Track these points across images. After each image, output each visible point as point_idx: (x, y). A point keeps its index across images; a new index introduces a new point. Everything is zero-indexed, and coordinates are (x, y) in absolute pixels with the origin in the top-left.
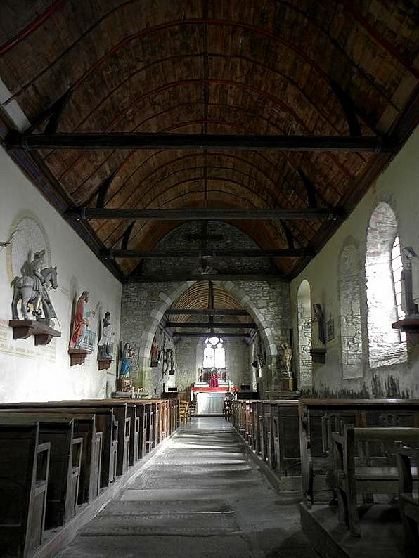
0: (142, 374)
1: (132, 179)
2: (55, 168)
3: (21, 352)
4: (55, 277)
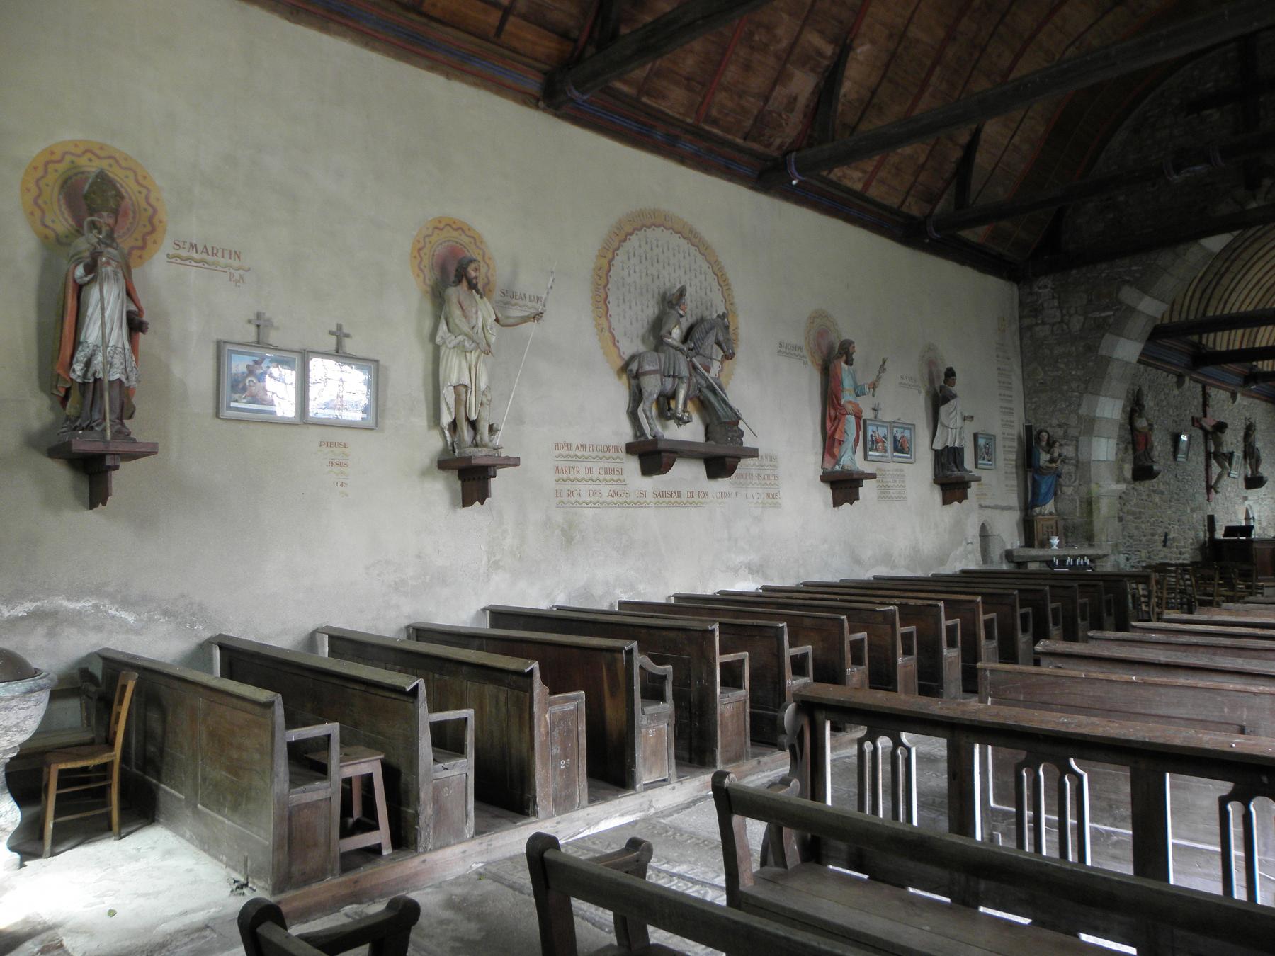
0: (1089, 504)
1: (913, 32)
2: (674, 101)
3: (669, 498)
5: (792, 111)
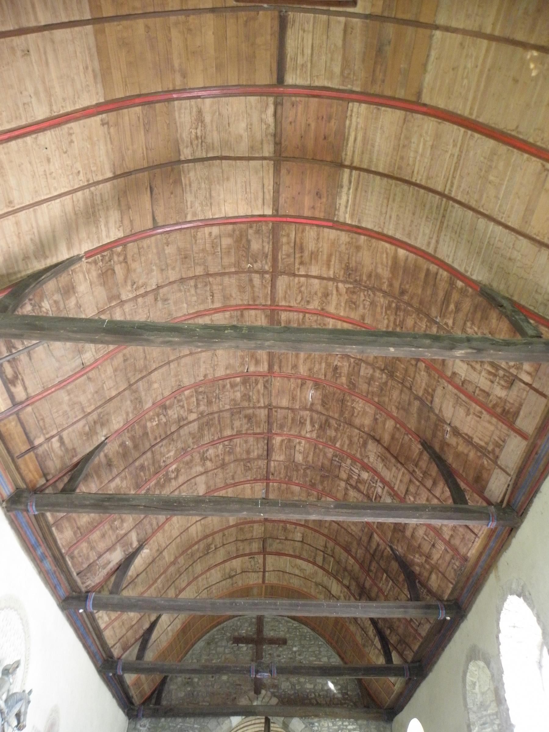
1: (165, 553)
4: (27, 708)
5: (104, 569)
